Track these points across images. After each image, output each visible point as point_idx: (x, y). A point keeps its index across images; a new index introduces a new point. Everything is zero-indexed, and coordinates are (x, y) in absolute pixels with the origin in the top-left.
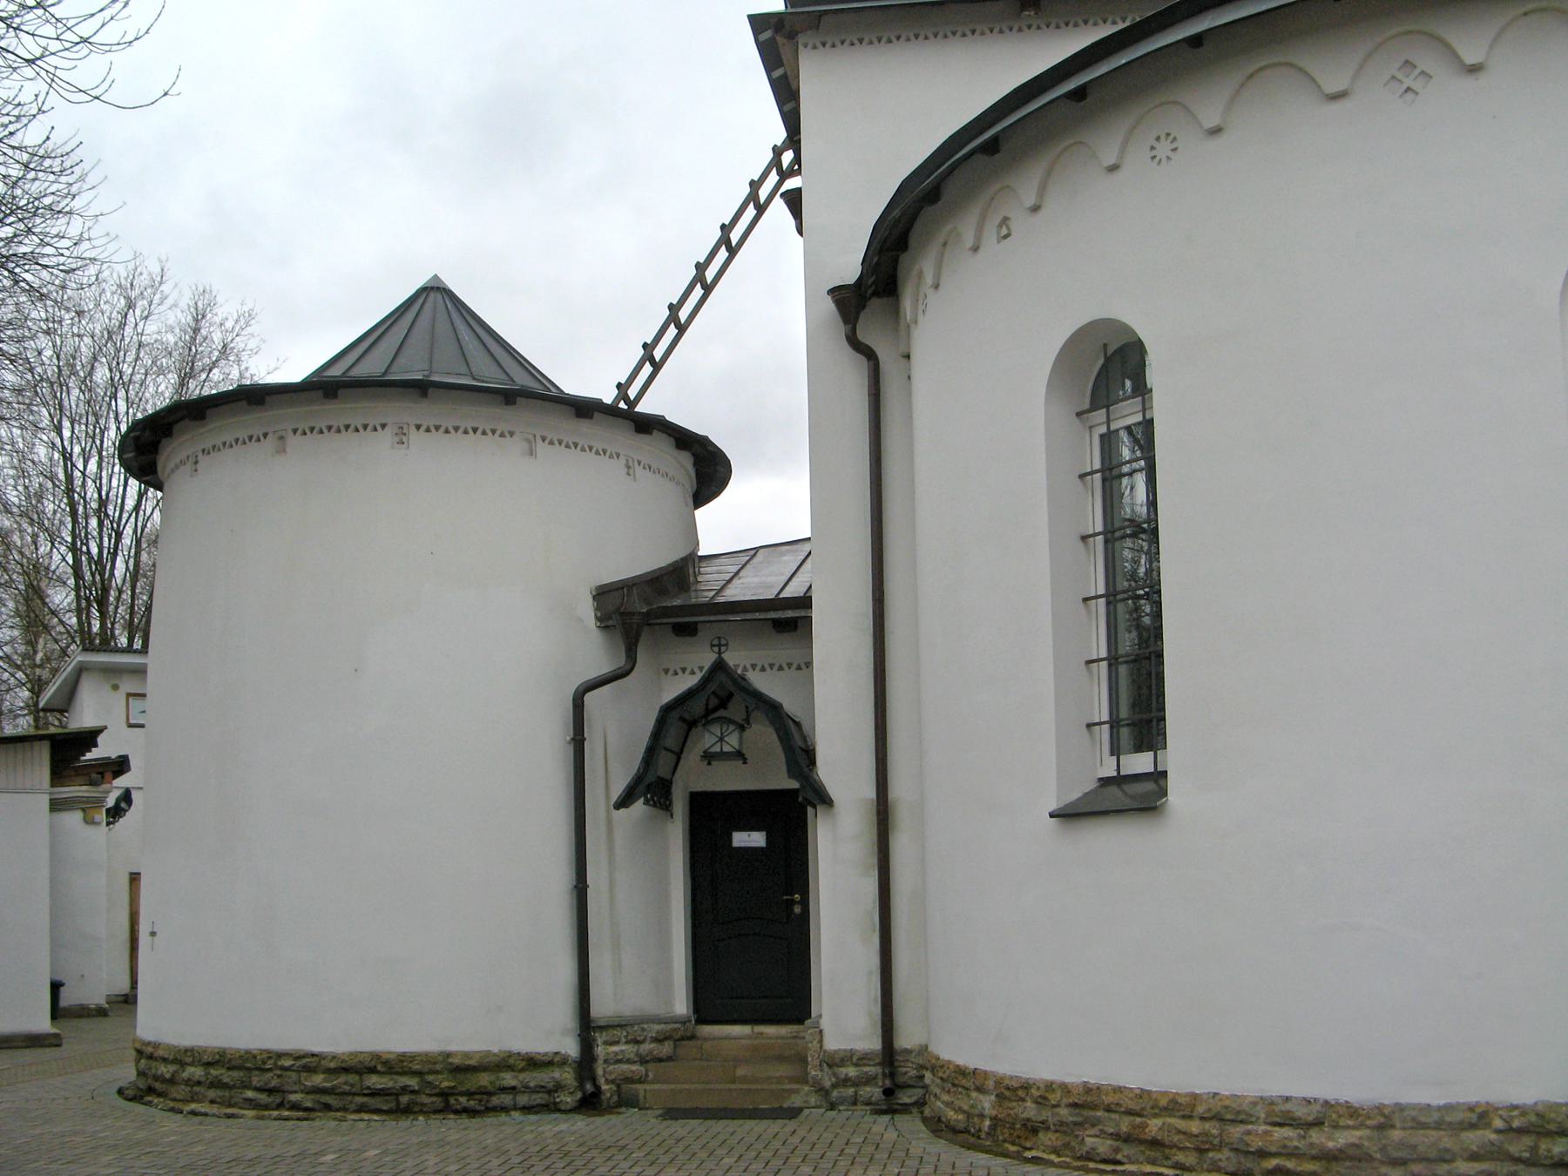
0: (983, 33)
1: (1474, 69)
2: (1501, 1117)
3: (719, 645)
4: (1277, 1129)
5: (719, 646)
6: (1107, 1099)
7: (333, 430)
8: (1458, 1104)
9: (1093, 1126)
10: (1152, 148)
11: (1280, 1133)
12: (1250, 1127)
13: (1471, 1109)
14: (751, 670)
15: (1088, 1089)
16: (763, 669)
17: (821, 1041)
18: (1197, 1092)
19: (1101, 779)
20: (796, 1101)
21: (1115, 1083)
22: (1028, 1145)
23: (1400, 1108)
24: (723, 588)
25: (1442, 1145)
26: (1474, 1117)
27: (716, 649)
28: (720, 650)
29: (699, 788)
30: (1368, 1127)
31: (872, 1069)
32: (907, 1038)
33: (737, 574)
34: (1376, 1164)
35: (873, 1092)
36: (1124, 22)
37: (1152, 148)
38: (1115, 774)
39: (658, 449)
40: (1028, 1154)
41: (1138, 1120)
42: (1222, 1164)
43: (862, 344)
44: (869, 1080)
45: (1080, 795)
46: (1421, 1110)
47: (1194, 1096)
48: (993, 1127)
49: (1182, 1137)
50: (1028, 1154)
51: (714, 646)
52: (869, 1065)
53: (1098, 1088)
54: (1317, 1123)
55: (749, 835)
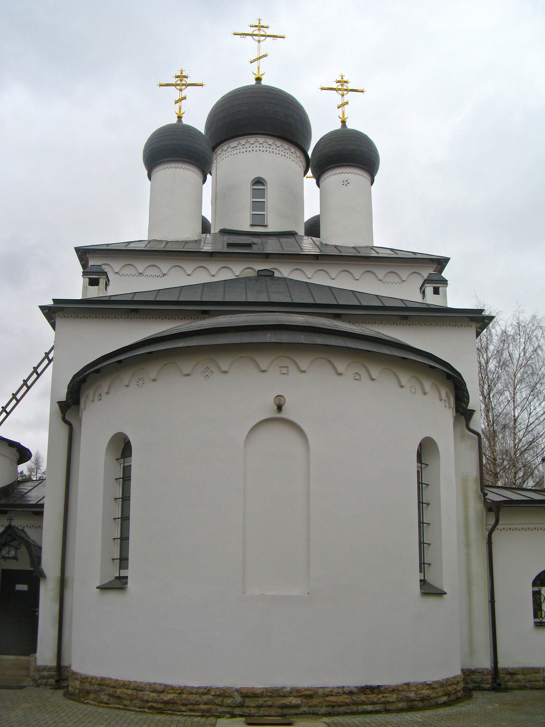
1: (225, 372)
2: (214, 691)
3: (10, 519)
4: (152, 693)
5: (10, 520)
6: (107, 682)
8: (202, 687)
9: (103, 691)
10: (138, 382)
11: (152, 694)
12: (145, 692)
13: (205, 688)
14: (26, 527)
15: (103, 679)
16: (30, 527)
17: (35, 662)
18: (131, 680)
19: (116, 577)
20: (25, 684)
21: (110, 677)
22: (86, 698)
23: (185, 687)
24: (28, 492)
25: (197, 700)
26: (206, 691)
27: (9, 521)
30: (177, 693)
32: (65, 663)
33: (30, 490)
34: (178, 705)
35: (52, 681)
37: (138, 382)
38: (118, 576)
40: (86, 701)
41: (115, 689)
42: (136, 705)
43: (67, 420)
44: (51, 677)
45: (108, 581)
46: (192, 688)
47: (130, 682)
48: (79, 692)
49: (126, 695)
50: (86, 701)
52: (52, 671)
53: (105, 679)
54: (163, 692)
55: (22, 586)
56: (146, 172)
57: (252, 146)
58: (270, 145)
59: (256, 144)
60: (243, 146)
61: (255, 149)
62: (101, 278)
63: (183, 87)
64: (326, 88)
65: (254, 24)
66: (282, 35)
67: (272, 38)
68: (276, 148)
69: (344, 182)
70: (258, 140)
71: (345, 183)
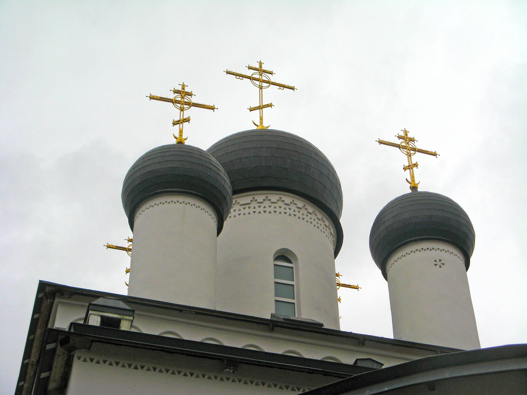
0: (197, 377)
7: (413, 252)
29: (273, 277)
36: (299, 391)
56: (126, 219)
57: (273, 205)
58: (300, 208)
59: (280, 204)
60: (260, 205)
61: (278, 210)
62: (123, 319)
63: (185, 106)
64: (387, 143)
65: (254, 66)
66: (291, 85)
67: (279, 87)
68: (308, 214)
69: (440, 260)
70: (283, 199)
71: (439, 263)
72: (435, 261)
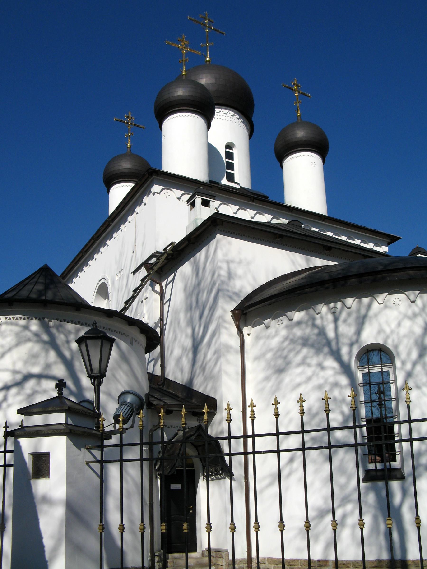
28: (200, 421)
31: (242, 565)
39: (134, 332)
51: (198, 420)
52: (241, 564)
55: (176, 485)
60: (218, 114)
61: (221, 117)
72: (312, 163)
